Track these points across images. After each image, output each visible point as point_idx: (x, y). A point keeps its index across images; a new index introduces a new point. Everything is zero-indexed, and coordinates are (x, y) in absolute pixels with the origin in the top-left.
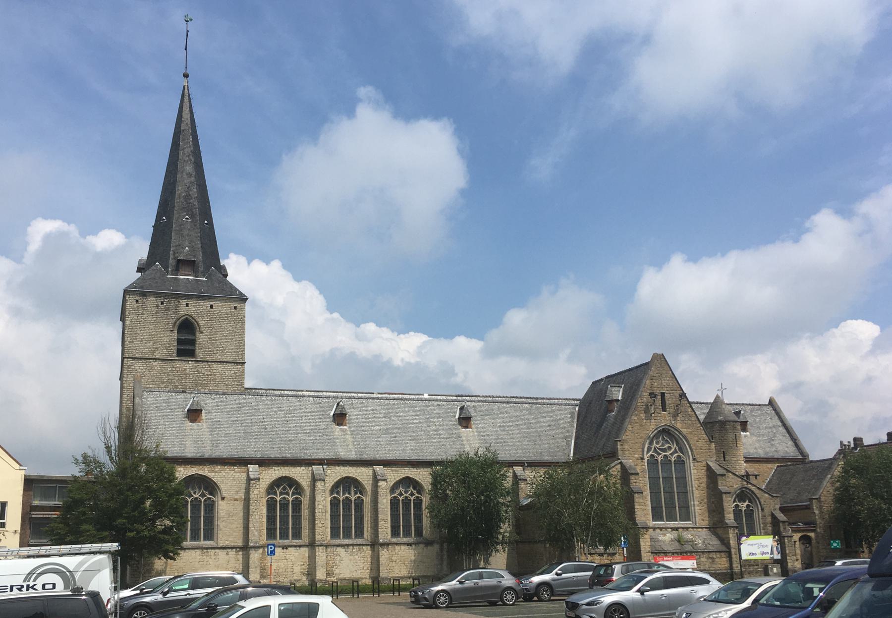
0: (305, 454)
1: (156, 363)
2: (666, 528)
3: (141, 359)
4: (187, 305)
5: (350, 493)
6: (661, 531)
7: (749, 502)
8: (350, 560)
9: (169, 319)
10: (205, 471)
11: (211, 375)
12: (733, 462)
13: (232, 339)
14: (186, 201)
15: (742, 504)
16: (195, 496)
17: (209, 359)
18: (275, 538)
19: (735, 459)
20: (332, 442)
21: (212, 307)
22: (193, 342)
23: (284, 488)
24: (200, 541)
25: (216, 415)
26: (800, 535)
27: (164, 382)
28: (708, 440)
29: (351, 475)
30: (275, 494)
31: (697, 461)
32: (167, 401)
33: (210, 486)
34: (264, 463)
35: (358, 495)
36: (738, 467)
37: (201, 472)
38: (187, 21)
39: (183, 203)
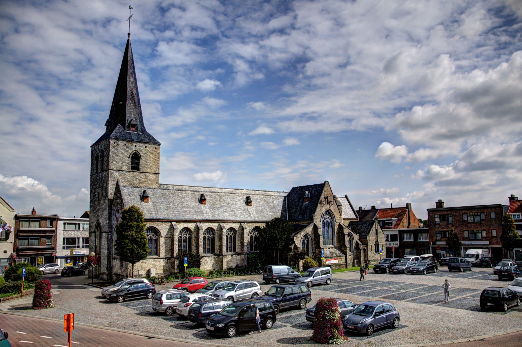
0: (193, 217)
1: (122, 173)
3: (116, 170)
4: (136, 146)
5: (210, 234)
8: (210, 262)
9: (128, 152)
10: (154, 225)
11: (146, 179)
13: (154, 163)
14: (131, 95)
16: (150, 236)
17: (145, 171)
18: (253, 250)
20: (202, 212)
21: (146, 147)
22: (138, 164)
23: (185, 232)
24: (152, 255)
25: (154, 199)
27: (126, 182)
29: (211, 227)
30: (186, 234)
32: (133, 192)
33: (156, 232)
37: (153, 225)
38: (130, 9)
39: (130, 96)
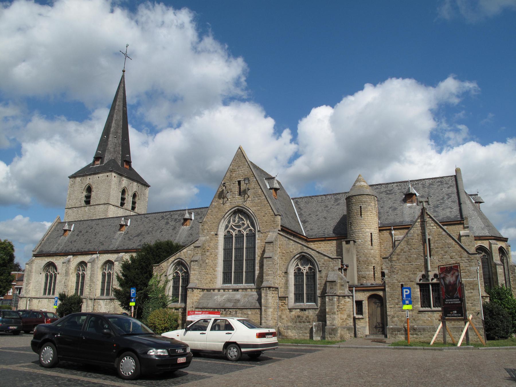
2: (228, 289)
6: (224, 291)
7: (310, 265)
12: (357, 230)
15: (304, 267)
19: (359, 228)
26: (368, 294)
28: (274, 214)
31: (261, 233)
34: (74, 254)
35: (110, 271)
36: (361, 235)
